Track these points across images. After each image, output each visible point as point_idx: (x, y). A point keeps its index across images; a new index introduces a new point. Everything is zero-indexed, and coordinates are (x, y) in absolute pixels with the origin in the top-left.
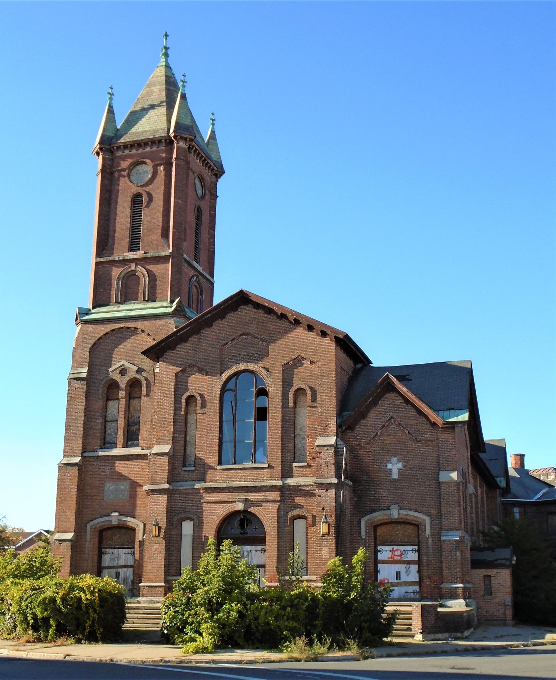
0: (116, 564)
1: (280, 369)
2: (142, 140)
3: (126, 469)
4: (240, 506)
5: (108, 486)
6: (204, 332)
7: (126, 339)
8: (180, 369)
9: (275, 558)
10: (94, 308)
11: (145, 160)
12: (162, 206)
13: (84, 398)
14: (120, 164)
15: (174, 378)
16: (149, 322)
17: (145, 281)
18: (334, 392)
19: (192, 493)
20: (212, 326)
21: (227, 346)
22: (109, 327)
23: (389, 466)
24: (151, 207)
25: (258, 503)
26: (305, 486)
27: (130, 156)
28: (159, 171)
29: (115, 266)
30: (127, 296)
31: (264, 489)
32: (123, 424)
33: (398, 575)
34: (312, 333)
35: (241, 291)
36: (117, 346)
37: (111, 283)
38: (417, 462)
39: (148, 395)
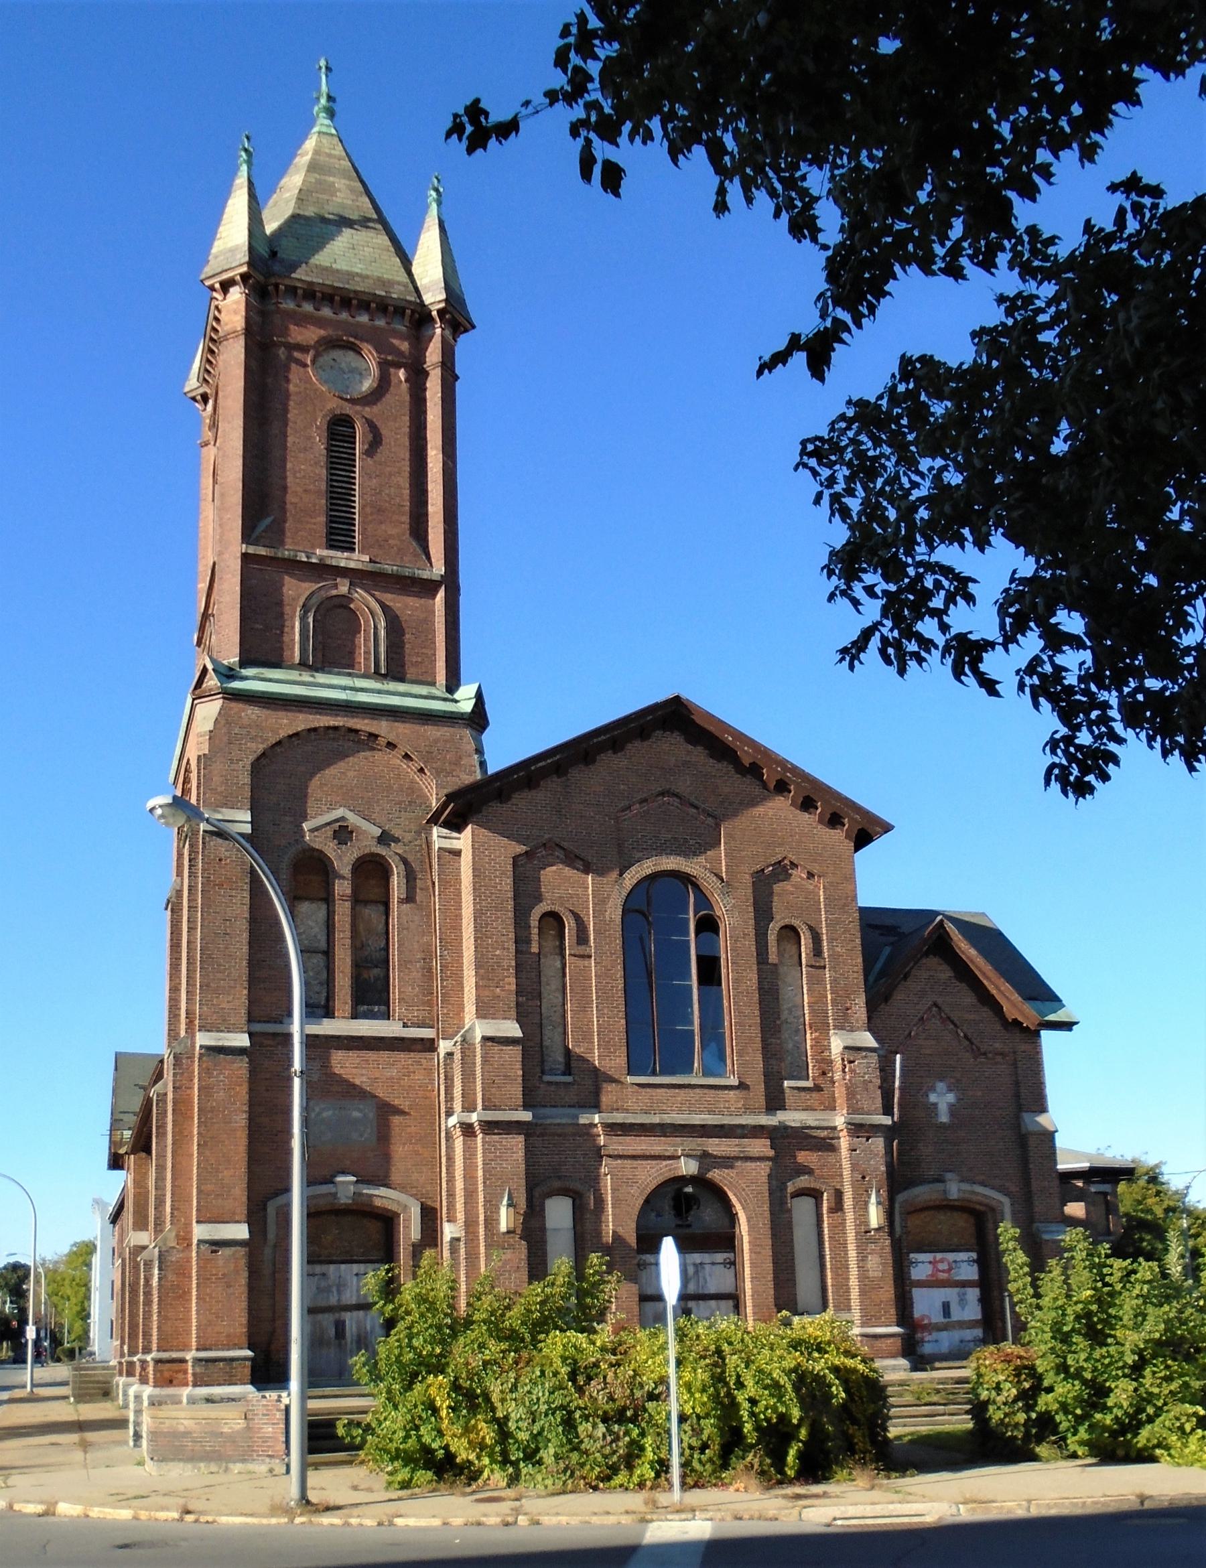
0: (333, 1300)
1: (747, 879)
2: (355, 292)
3: (364, 1072)
4: (687, 1167)
5: (317, 1109)
6: (575, 774)
7: (342, 756)
8: (524, 848)
9: (770, 1277)
10: (244, 663)
11: (357, 342)
12: (408, 463)
13: (247, 887)
14: (287, 328)
15: (510, 868)
16: (407, 725)
17: (376, 627)
18: (858, 941)
19: (574, 1135)
20: (594, 761)
21: (628, 814)
22: (302, 721)
23: (933, 1098)
24: (377, 457)
25: (727, 1162)
26: (818, 1128)
27: (320, 323)
28: (394, 380)
29: (292, 575)
30: (331, 652)
31: (739, 1131)
32: (349, 960)
33: (946, 1307)
34: (807, 815)
35: (677, 698)
36: (320, 769)
37: (282, 614)
38: (980, 1093)
39: (409, 898)
